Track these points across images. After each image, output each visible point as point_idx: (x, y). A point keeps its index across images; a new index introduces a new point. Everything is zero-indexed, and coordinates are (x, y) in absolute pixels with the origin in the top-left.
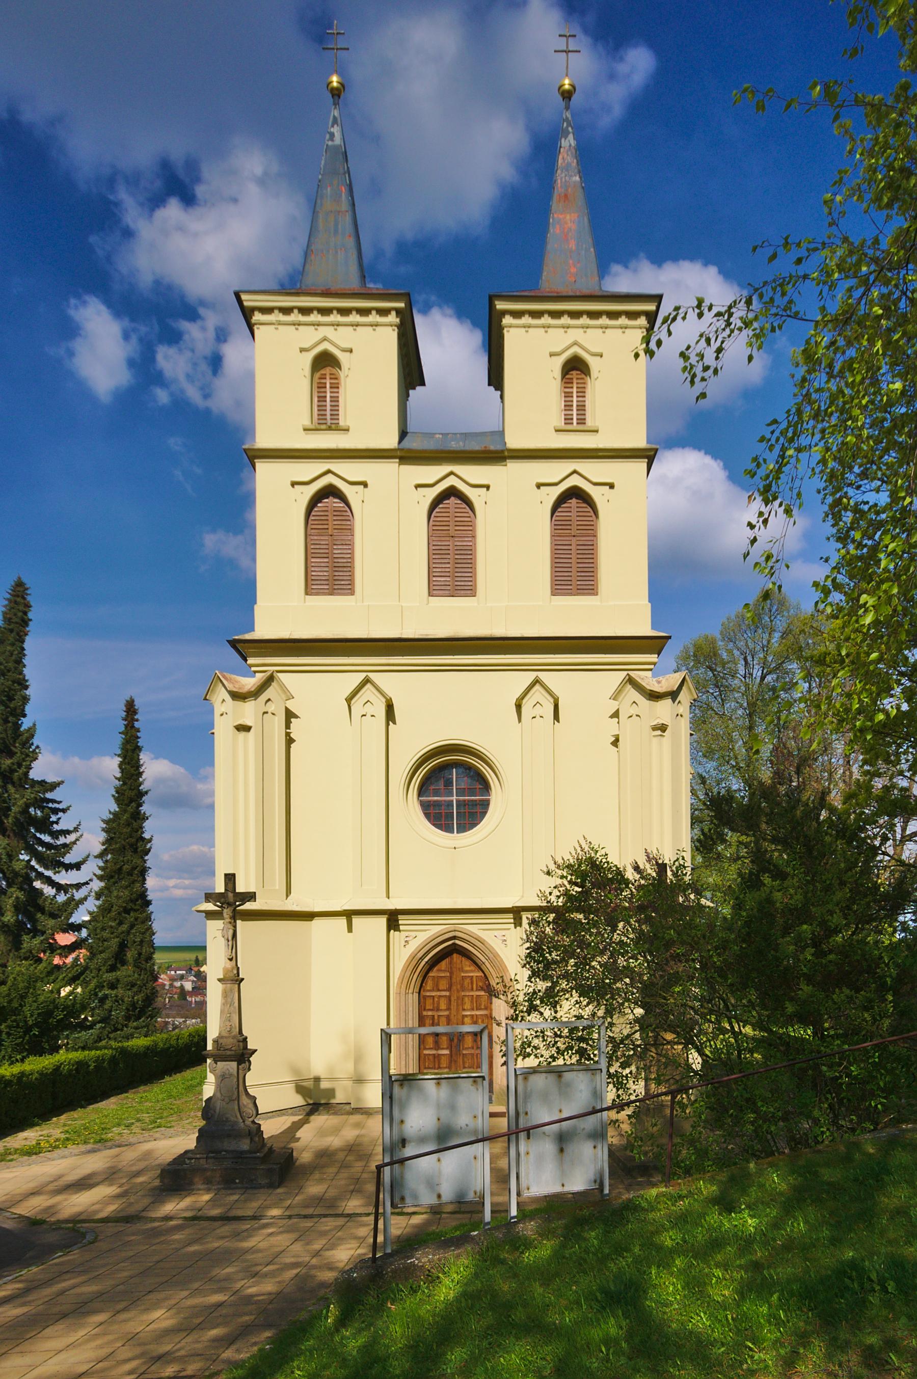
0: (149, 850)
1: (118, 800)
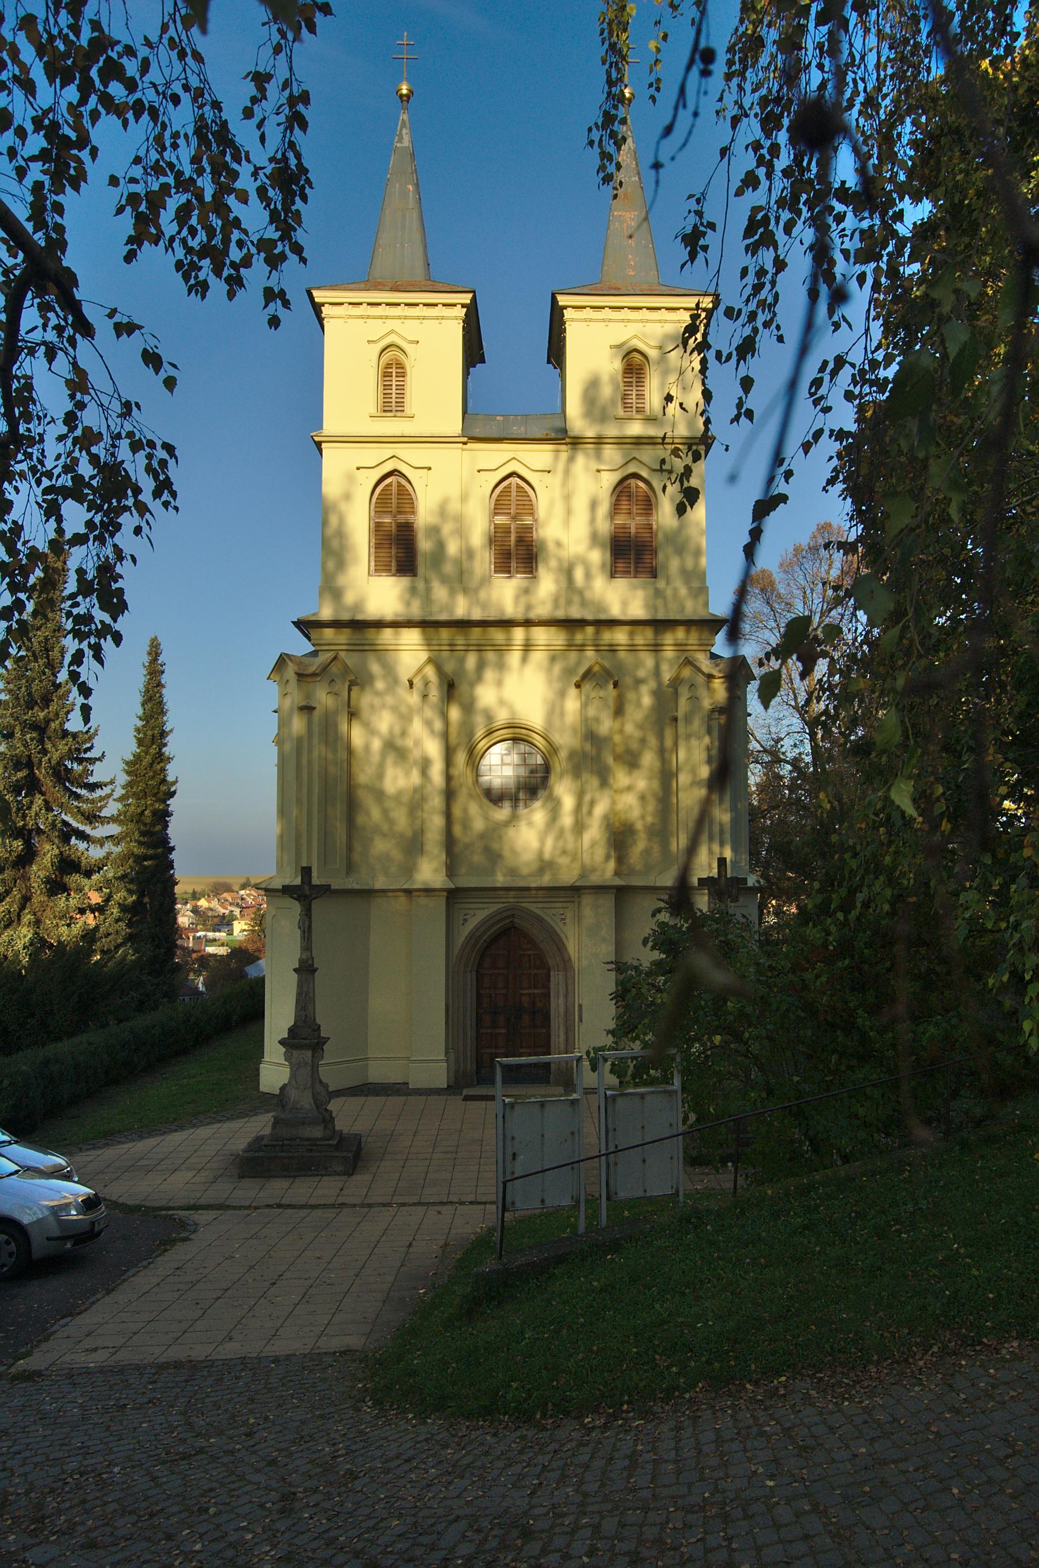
0: (174, 792)
1: (140, 742)
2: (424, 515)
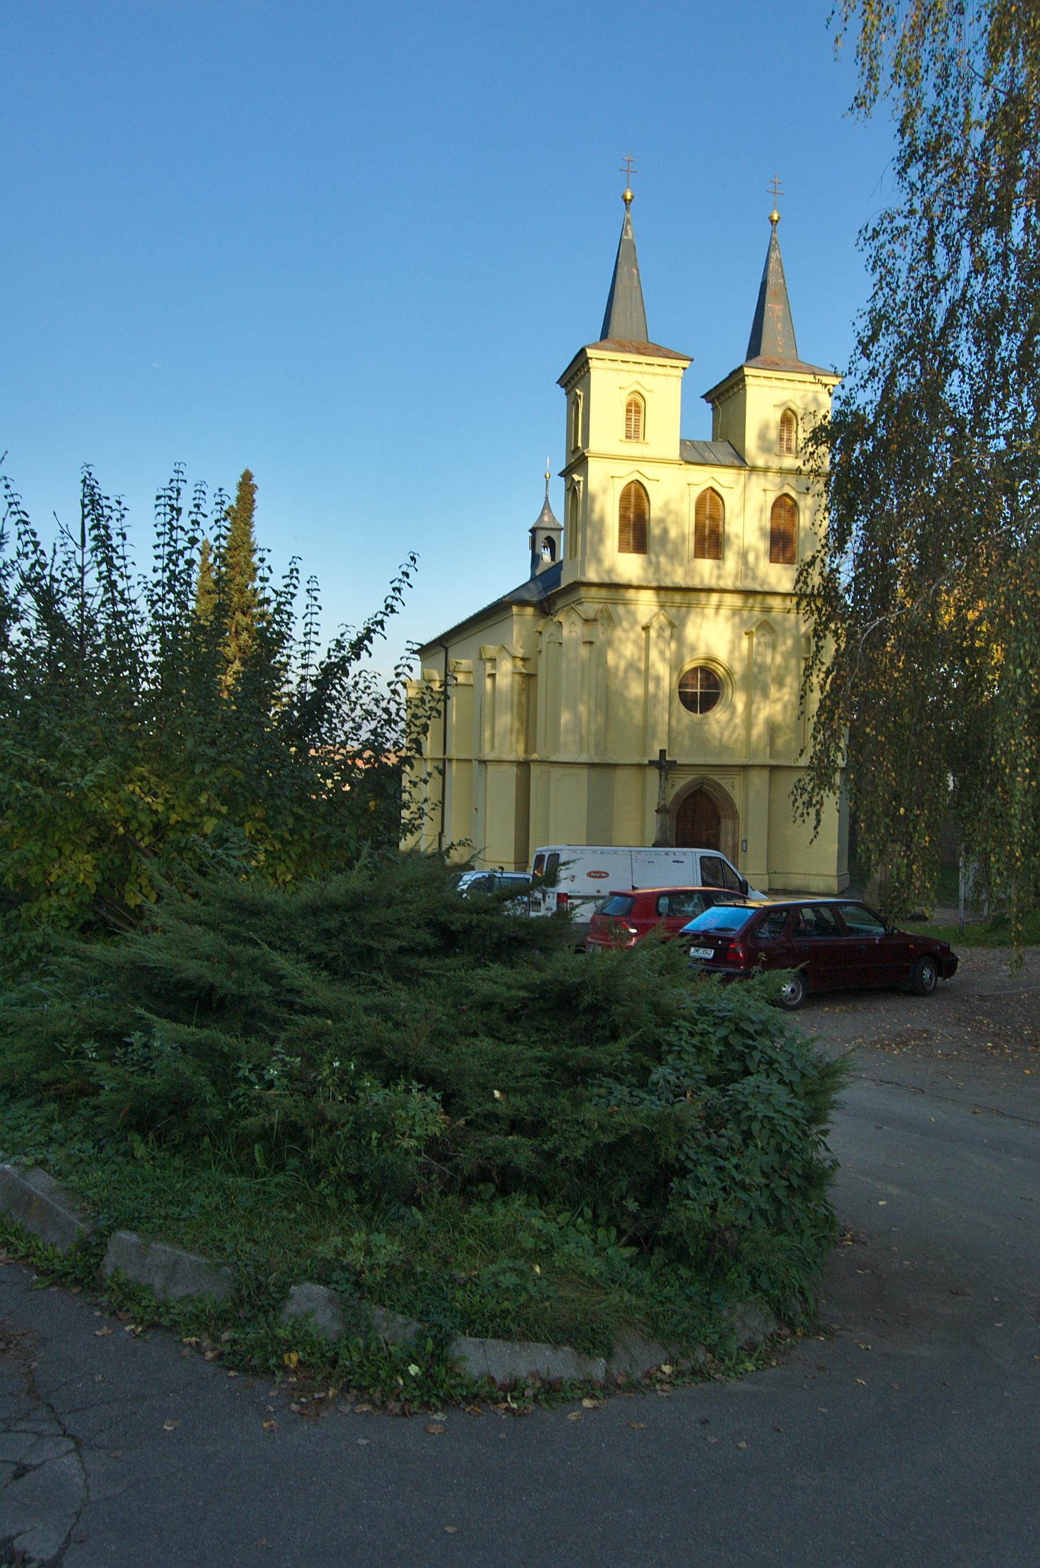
2: (655, 511)
